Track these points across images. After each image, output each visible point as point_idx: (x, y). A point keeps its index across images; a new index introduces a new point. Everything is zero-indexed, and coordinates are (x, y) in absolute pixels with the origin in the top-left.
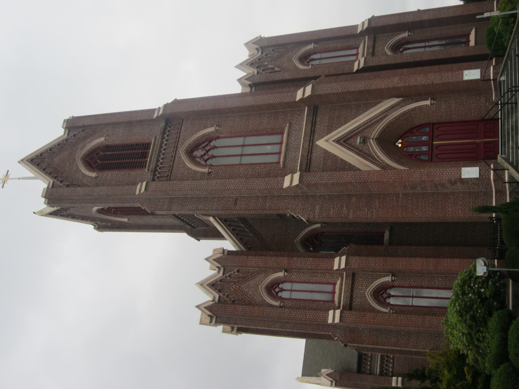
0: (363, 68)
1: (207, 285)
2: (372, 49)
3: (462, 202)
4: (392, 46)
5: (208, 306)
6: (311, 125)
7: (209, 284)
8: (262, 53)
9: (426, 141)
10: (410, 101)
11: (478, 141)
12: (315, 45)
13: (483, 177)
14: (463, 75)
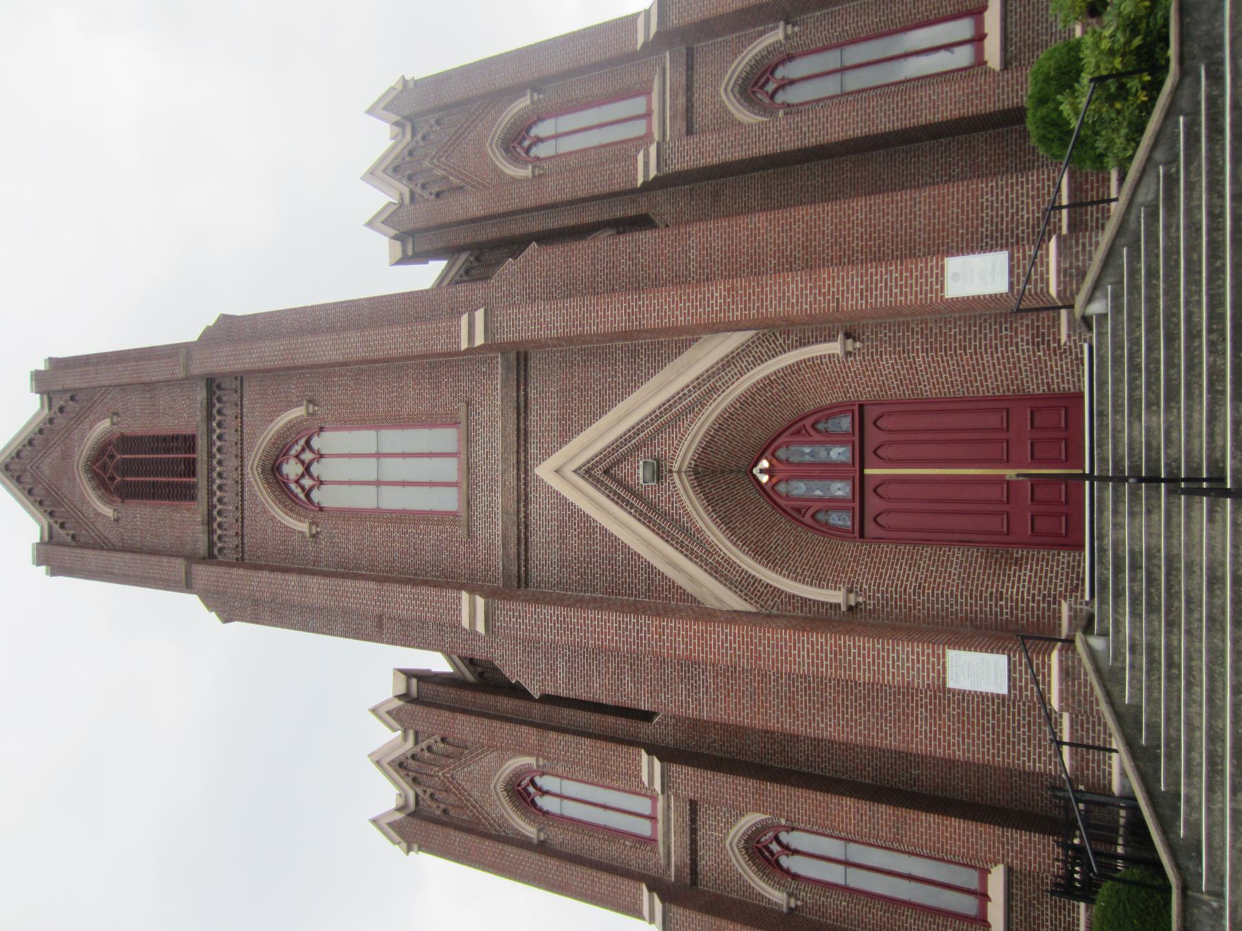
0: (656, 178)
1: (389, 764)
2: (685, 98)
3: (959, 708)
4: (740, 82)
5: (395, 822)
6: (515, 416)
7: (393, 761)
8: (414, 134)
9: (843, 464)
10: (781, 341)
11: (1010, 473)
12: (536, 96)
13: (1024, 693)
14: (943, 275)
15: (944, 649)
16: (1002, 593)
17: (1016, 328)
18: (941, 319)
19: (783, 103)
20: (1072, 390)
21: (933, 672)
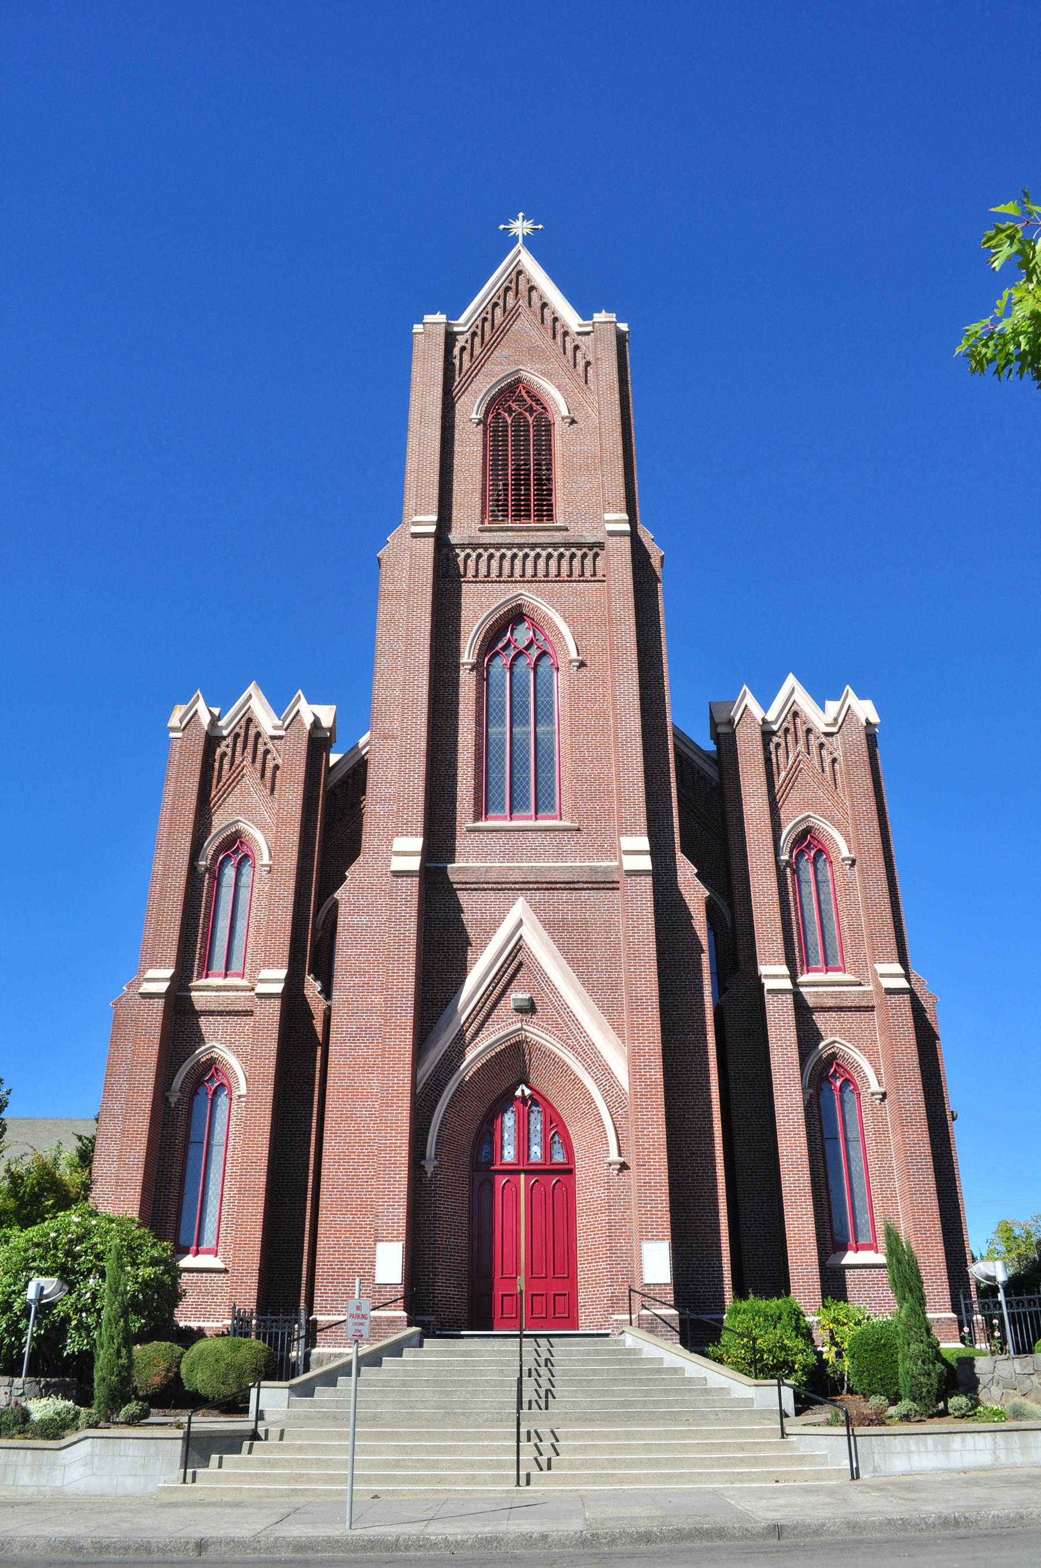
15: (402, 1240)
19: (821, 1089)
20: (580, 1322)
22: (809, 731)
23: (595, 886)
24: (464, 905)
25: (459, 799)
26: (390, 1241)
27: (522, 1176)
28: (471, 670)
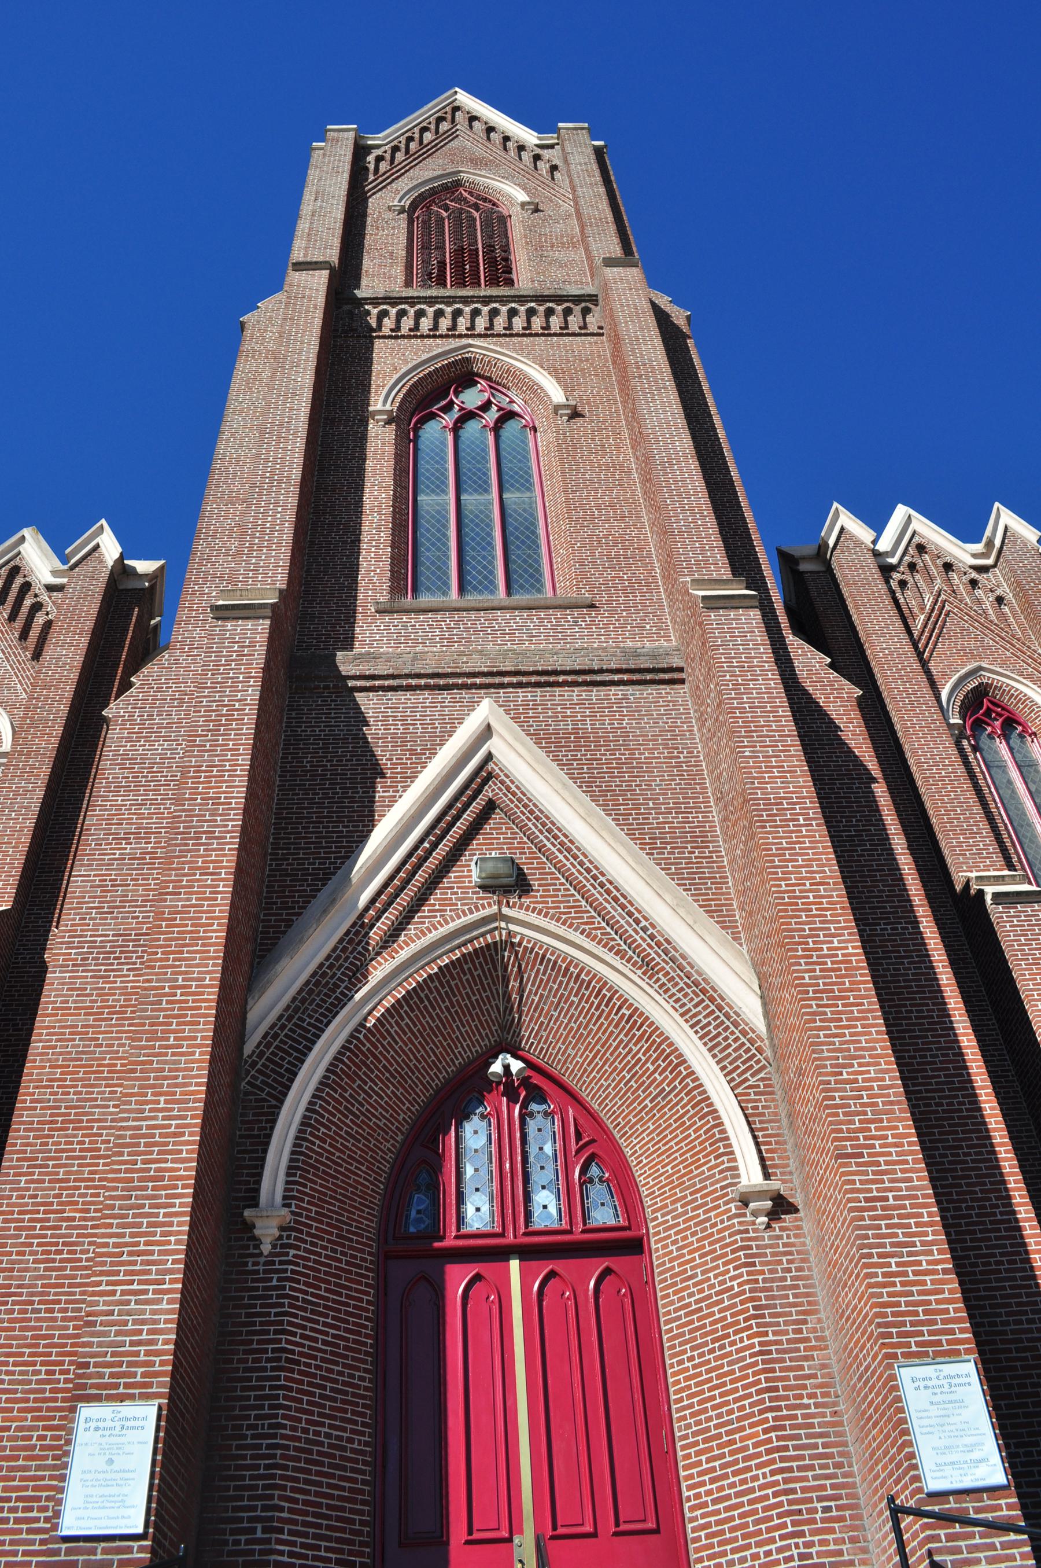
3: (43, 1448)
16: (281, 1531)
17: (832, 1531)
18: (830, 1376)
21: (112, 1375)
22: (948, 567)
23: (635, 677)
24: (370, 714)
25: (362, 571)
26: (122, 1398)
27: (514, 1265)
28: (388, 422)
